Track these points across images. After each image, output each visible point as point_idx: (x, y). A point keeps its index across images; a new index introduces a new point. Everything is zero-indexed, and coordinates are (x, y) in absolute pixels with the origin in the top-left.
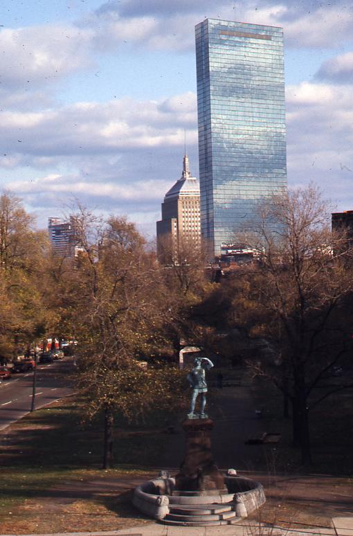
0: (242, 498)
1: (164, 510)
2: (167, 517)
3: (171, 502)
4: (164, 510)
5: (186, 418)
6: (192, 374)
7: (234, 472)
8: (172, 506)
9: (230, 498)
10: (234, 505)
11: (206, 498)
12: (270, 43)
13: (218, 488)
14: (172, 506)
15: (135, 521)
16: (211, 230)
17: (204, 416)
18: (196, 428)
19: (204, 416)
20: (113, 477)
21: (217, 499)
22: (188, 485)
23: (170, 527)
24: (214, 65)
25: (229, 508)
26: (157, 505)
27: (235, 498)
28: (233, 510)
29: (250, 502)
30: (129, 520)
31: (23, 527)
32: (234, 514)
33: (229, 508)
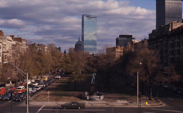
0: (101, 97)
1: (88, 98)
2: (88, 100)
3: (89, 97)
4: (88, 98)
5: (91, 83)
6: (92, 76)
7: (98, 92)
8: (89, 98)
9: (99, 96)
10: (100, 98)
11: (95, 97)
12: (94, 19)
13: (96, 95)
14: (89, 98)
15: (83, 100)
16: (119, 51)
17: (94, 83)
18: (92, 85)
19: (94, 83)
20: (77, 93)
21: (97, 97)
22: (91, 94)
23: (89, 101)
24: (81, 26)
25: (99, 98)
26: (87, 97)
27: (100, 97)
28: (99, 99)
29: (102, 97)
30: (82, 100)
31: (64, 101)
32: (100, 99)
33: (99, 98)
